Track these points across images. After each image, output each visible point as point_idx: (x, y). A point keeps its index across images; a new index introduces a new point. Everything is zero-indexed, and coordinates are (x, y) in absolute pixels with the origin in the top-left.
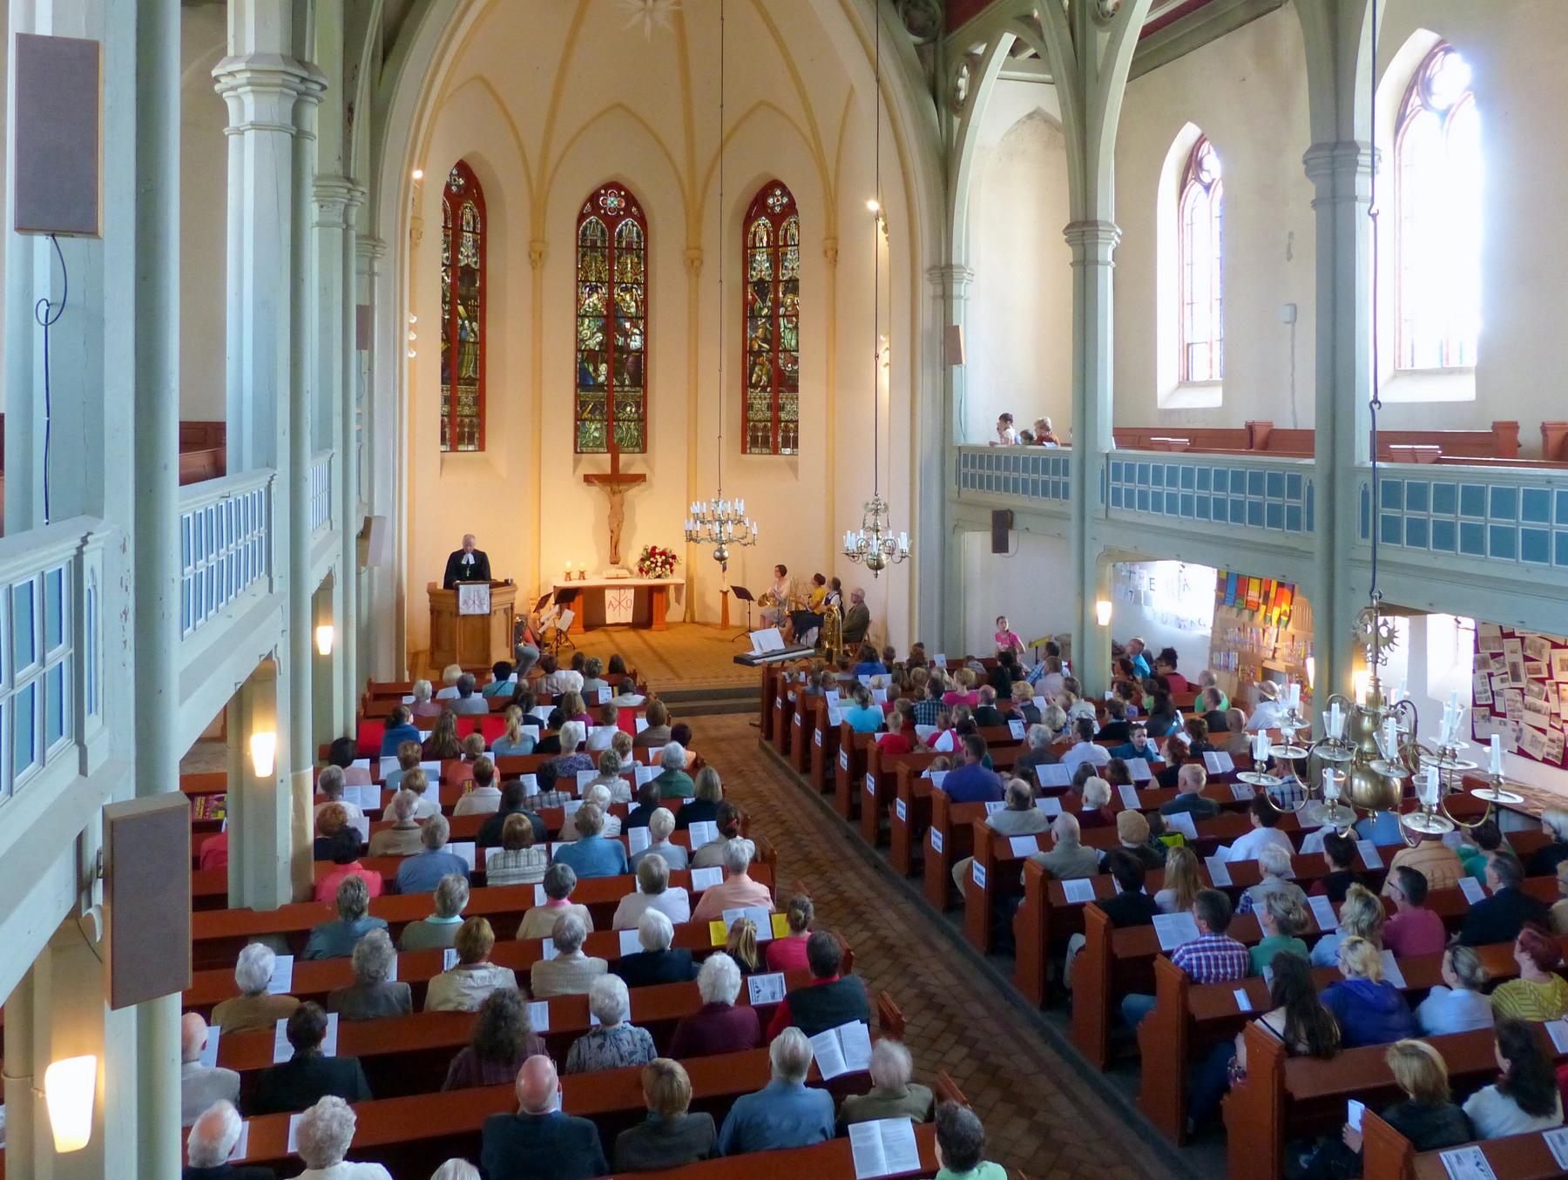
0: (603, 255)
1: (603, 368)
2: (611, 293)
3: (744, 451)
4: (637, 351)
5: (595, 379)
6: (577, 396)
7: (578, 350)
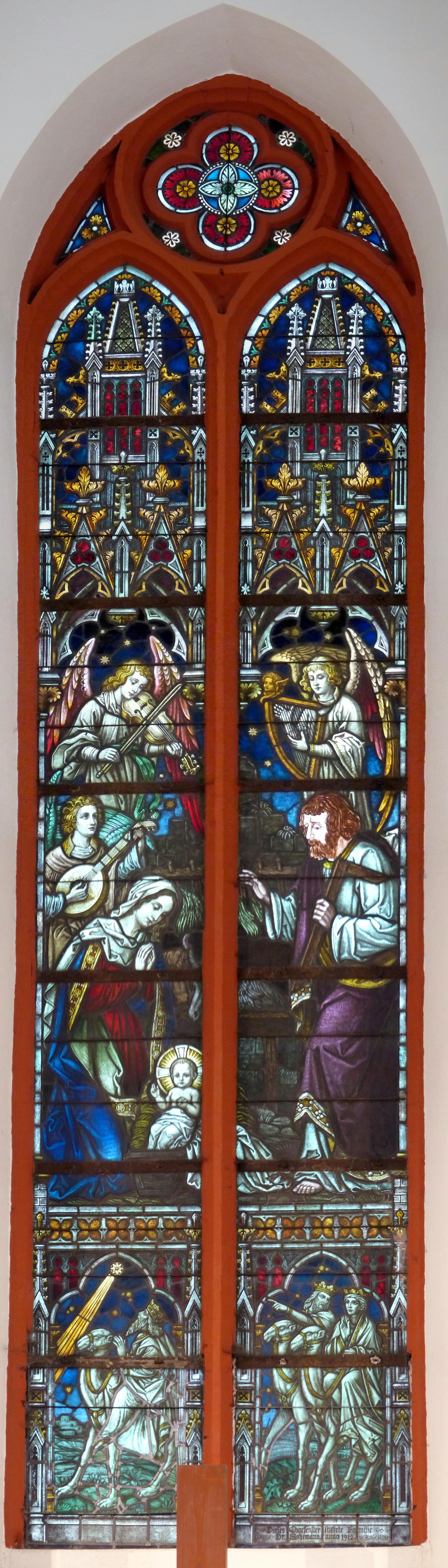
0: (176, 463)
1: (177, 1069)
2: (223, 659)
3: (19, 1539)
4: (182, 1004)
5: (128, 1133)
6: (26, 1229)
7: (34, 974)
